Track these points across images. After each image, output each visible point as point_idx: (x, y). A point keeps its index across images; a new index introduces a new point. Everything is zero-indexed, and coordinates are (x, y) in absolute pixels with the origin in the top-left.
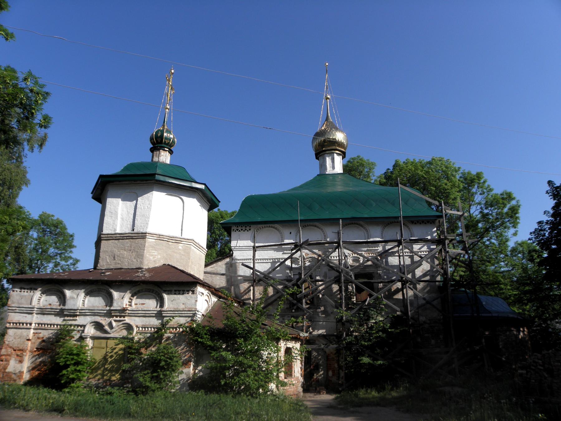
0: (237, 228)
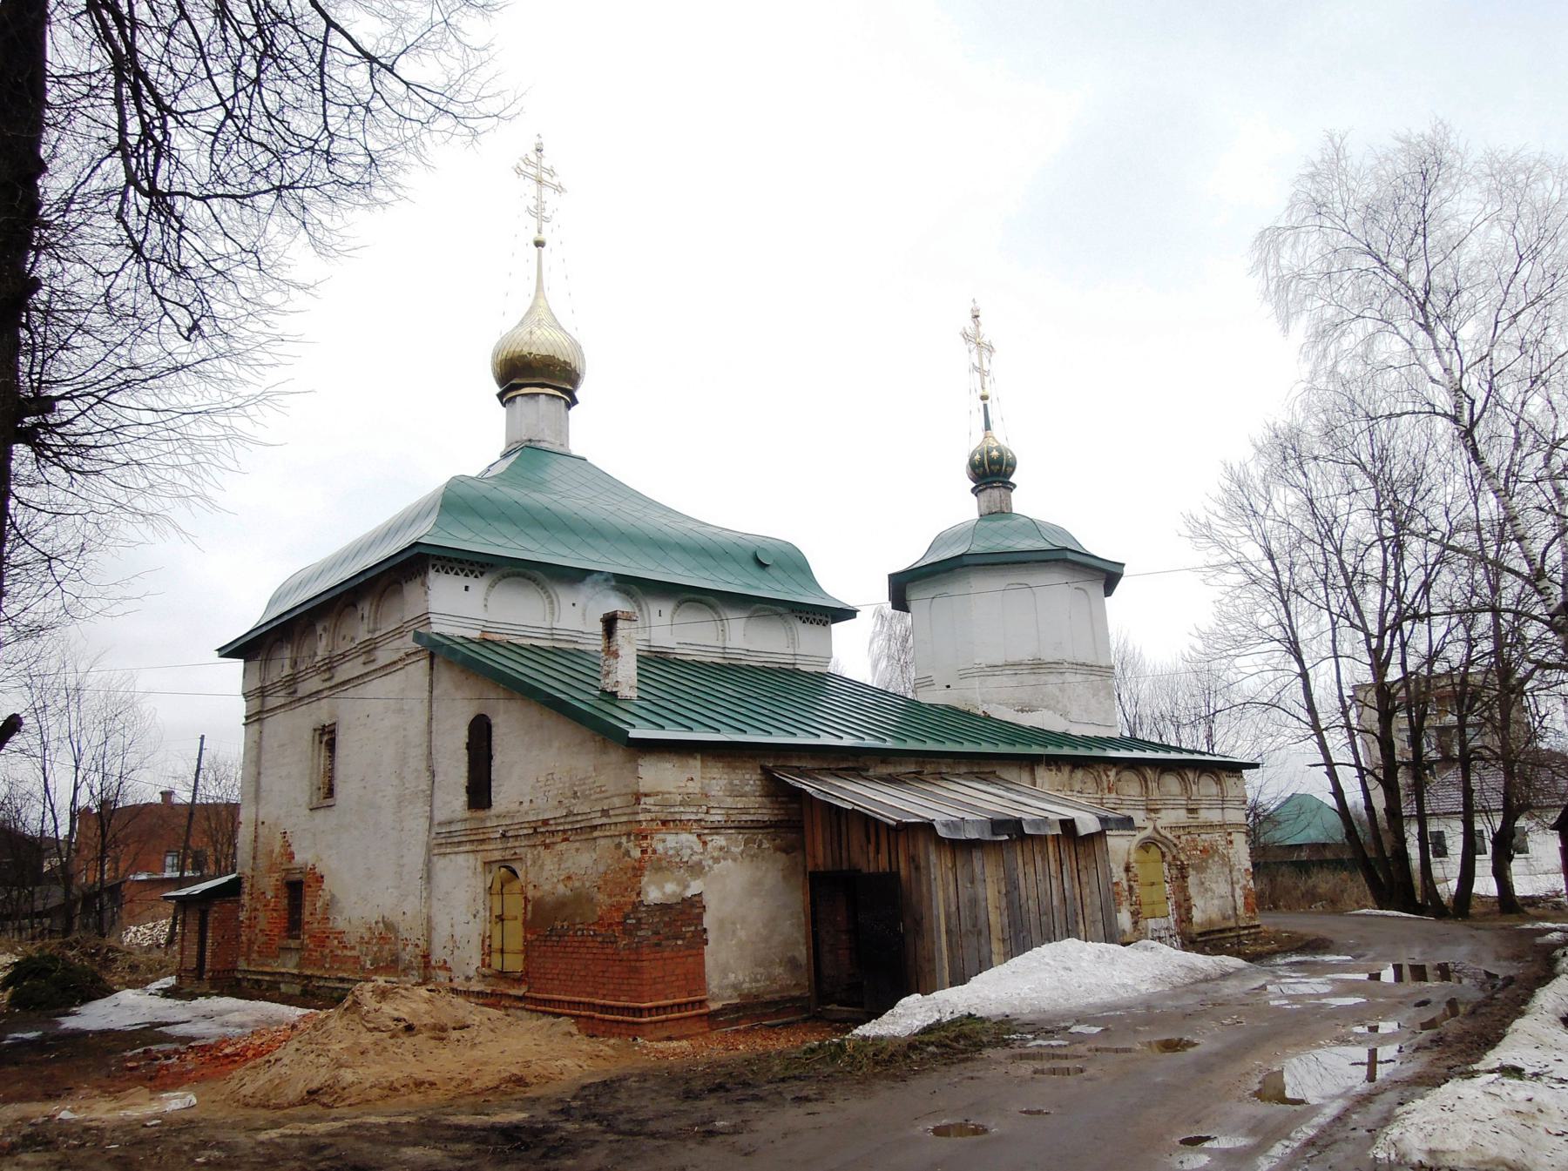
0: (463, 567)
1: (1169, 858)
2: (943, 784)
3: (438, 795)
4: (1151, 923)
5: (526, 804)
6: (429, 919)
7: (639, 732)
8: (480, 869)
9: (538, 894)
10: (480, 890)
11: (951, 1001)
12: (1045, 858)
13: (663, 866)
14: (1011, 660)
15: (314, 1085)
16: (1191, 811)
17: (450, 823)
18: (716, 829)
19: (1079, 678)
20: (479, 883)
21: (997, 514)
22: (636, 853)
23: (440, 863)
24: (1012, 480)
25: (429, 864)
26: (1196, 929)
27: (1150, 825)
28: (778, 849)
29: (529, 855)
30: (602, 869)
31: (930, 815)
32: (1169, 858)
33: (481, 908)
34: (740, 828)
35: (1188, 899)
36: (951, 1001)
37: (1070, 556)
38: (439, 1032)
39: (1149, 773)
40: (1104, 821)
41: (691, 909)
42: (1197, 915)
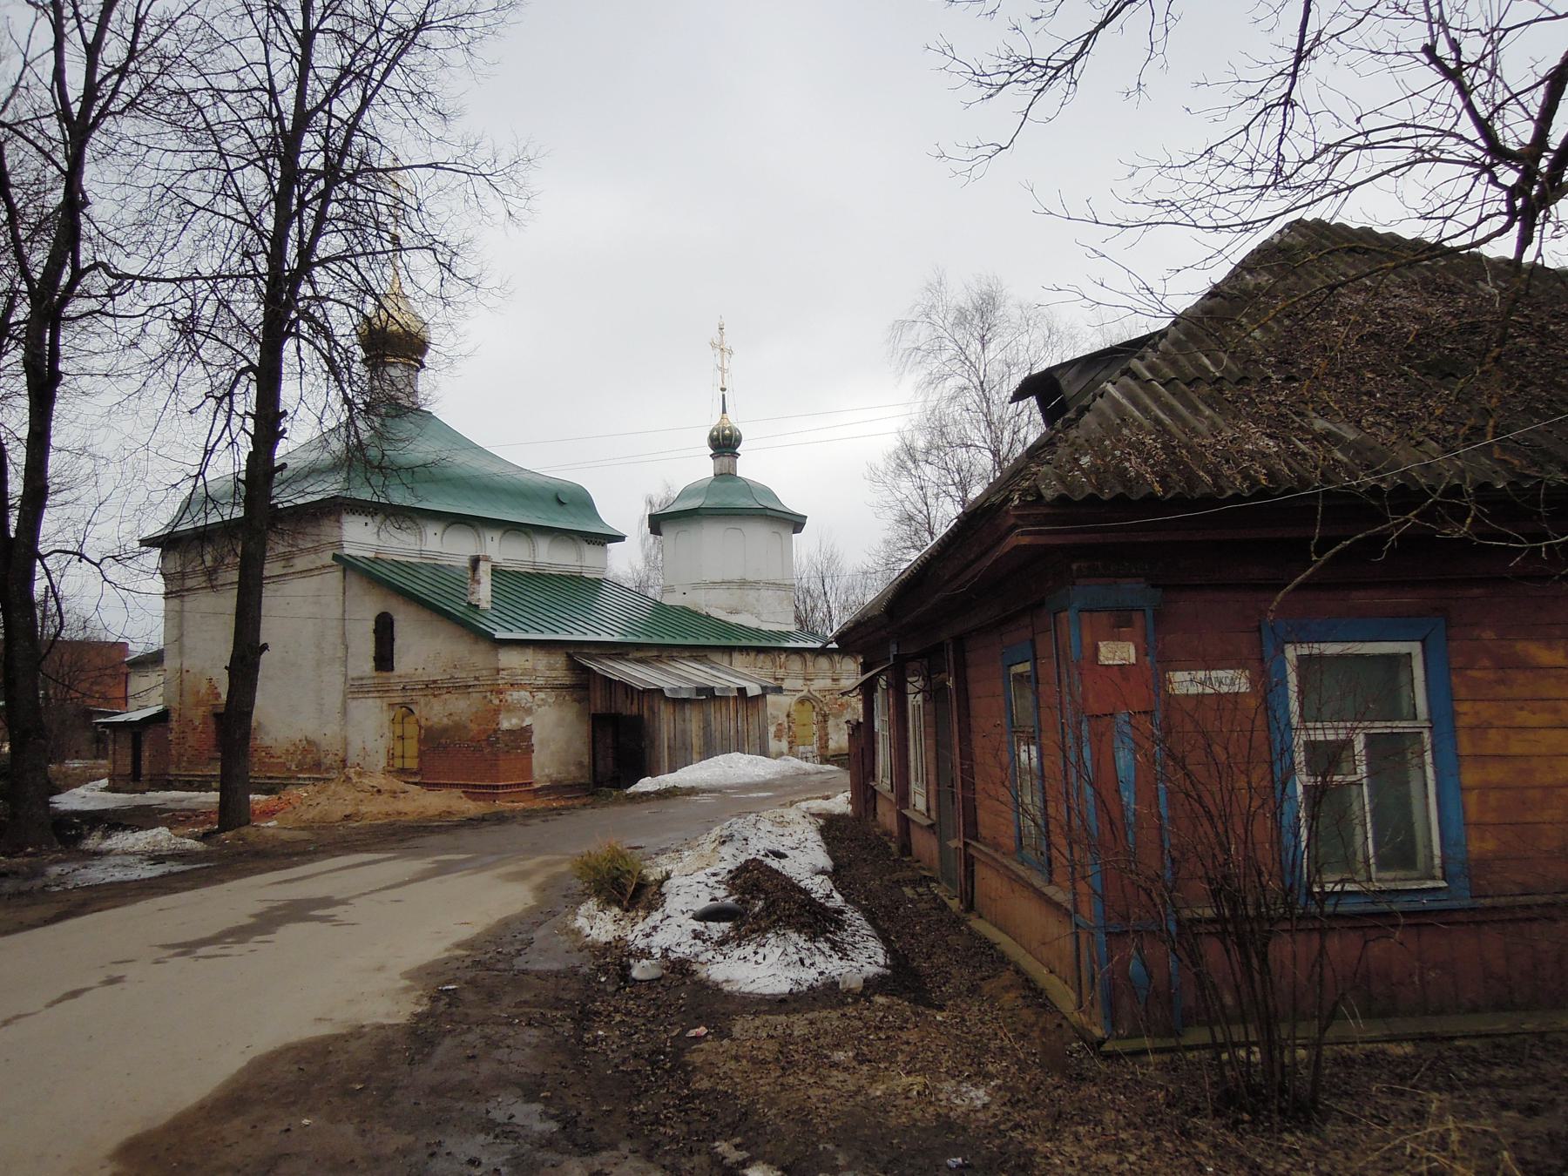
1: (817, 709)
2: (673, 663)
3: (351, 660)
4: (801, 749)
5: (420, 671)
6: (345, 739)
7: (498, 635)
8: (385, 708)
9: (429, 723)
10: (387, 723)
11: (667, 780)
12: (728, 709)
13: (511, 709)
14: (726, 579)
15: (347, 813)
16: (834, 680)
17: (362, 679)
18: (540, 689)
19: (770, 592)
20: (386, 717)
21: (726, 476)
22: (496, 702)
23: (353, 704)
24: (738, 450)
25: (344, 703)
26: (830, 753)
27: (806, 689)
28: (575, 700)
29: (422, 701)
30: (474, 710)
31: (661, 684)
32: (817, 709)
33: (386, 731)
34: (553, 688)
35: (827, 734)
36: (667, 780)
37: (769, 513)
38: (394, 794)
39: (808, 656)
40: (763, 688)
41: (524, 733)
42: (832, 745)
